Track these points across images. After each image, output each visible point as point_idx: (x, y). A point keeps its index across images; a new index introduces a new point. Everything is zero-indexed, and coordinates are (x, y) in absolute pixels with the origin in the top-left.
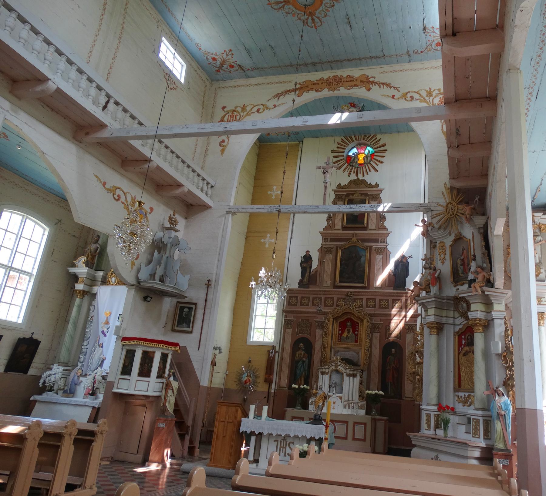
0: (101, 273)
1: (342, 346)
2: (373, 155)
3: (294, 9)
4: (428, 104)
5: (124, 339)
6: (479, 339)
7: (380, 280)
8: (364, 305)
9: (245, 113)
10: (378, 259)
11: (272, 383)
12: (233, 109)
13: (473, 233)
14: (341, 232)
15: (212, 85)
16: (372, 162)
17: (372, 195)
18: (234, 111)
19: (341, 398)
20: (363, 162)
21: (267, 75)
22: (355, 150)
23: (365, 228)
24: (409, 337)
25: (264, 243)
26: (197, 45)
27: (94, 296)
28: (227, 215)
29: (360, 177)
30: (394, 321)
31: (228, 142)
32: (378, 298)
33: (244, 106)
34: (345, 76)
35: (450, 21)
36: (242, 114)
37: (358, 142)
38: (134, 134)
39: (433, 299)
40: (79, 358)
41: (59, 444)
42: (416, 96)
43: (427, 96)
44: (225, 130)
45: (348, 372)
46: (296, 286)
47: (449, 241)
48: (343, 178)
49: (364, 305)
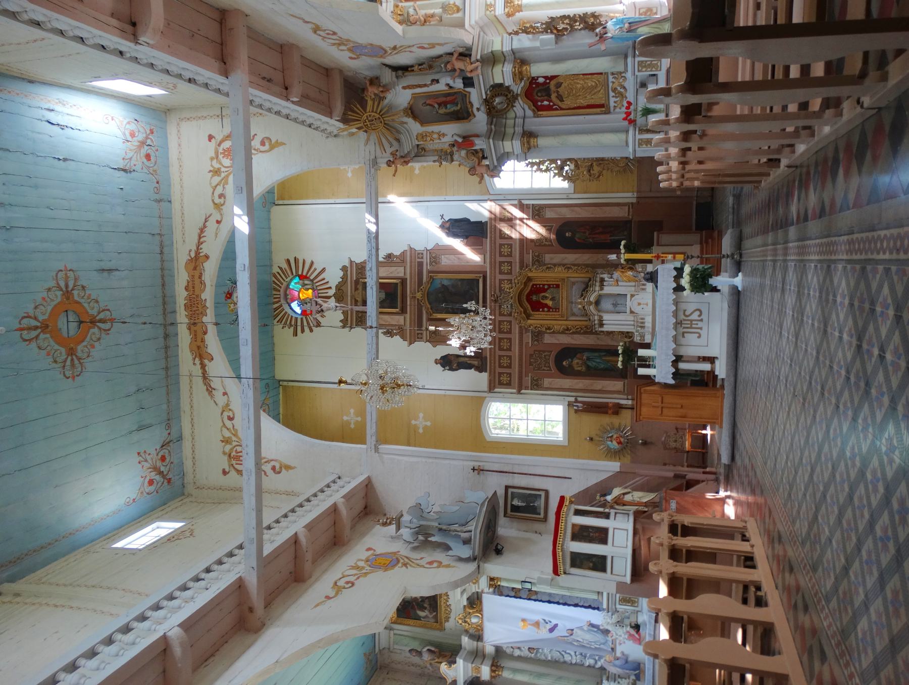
0: (465, 640)
1: (565, 306)
2: (302, 277)
3: (84, 344)
4: (229, 174)
5: (556, 572)
6: (539, 70)
7: (472, 256)
8: (509, 277)
9: (234, 438)
10: (446, 261)
11: (618, 404)
12: (226, 458)
13: (404, 88)
14: (408, 316)
15: (190, 495)
16: (311, 278)
17: (357, 274)
18: (230, 455)
19: (632, 296)
20: (310, 291)
21: (178, 408)
22: (295, 305)
23: (403, 281)
24: (549, 214)
25: (425, 428)
26: (128, 504)
27: (499, 650)
28: (380, 451)
29: (331, 292)
30: (529, 234)
31: (275, 460)
32: (499, 259)
33: (223, 441)
34: (185, 293)
35: (114, 22)
36: (234, 444)
37: (283, 301)
38: (254, 531)
39: (491, 141)
40: (589, 666)
41: (684, 551)
42: (219, 190)
43: (219, 175)
44: (251, 387)
45: (597, 288)
46: (485, 376)
47: (415, 127)
48: (333, 315)
49: (509, 277)
